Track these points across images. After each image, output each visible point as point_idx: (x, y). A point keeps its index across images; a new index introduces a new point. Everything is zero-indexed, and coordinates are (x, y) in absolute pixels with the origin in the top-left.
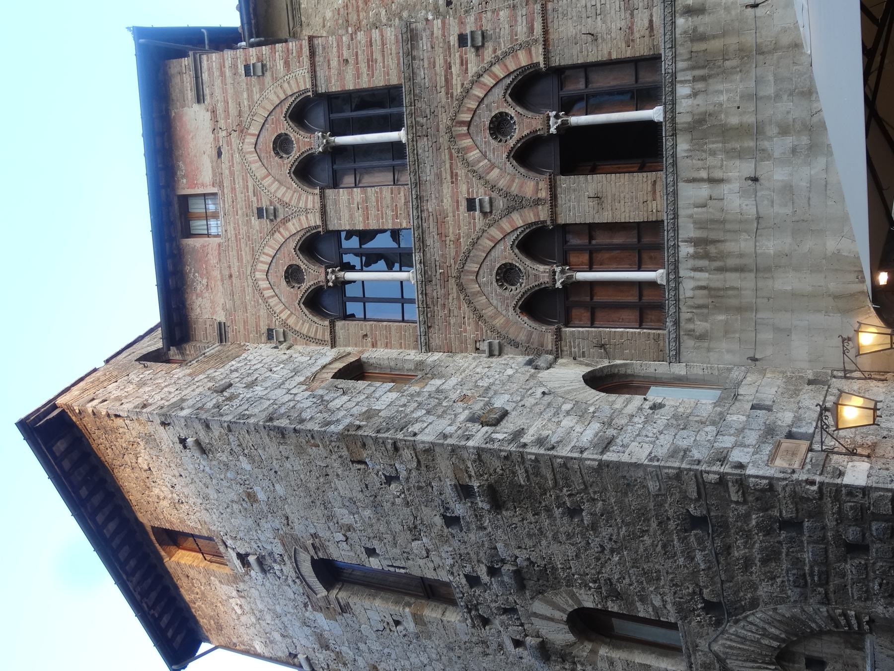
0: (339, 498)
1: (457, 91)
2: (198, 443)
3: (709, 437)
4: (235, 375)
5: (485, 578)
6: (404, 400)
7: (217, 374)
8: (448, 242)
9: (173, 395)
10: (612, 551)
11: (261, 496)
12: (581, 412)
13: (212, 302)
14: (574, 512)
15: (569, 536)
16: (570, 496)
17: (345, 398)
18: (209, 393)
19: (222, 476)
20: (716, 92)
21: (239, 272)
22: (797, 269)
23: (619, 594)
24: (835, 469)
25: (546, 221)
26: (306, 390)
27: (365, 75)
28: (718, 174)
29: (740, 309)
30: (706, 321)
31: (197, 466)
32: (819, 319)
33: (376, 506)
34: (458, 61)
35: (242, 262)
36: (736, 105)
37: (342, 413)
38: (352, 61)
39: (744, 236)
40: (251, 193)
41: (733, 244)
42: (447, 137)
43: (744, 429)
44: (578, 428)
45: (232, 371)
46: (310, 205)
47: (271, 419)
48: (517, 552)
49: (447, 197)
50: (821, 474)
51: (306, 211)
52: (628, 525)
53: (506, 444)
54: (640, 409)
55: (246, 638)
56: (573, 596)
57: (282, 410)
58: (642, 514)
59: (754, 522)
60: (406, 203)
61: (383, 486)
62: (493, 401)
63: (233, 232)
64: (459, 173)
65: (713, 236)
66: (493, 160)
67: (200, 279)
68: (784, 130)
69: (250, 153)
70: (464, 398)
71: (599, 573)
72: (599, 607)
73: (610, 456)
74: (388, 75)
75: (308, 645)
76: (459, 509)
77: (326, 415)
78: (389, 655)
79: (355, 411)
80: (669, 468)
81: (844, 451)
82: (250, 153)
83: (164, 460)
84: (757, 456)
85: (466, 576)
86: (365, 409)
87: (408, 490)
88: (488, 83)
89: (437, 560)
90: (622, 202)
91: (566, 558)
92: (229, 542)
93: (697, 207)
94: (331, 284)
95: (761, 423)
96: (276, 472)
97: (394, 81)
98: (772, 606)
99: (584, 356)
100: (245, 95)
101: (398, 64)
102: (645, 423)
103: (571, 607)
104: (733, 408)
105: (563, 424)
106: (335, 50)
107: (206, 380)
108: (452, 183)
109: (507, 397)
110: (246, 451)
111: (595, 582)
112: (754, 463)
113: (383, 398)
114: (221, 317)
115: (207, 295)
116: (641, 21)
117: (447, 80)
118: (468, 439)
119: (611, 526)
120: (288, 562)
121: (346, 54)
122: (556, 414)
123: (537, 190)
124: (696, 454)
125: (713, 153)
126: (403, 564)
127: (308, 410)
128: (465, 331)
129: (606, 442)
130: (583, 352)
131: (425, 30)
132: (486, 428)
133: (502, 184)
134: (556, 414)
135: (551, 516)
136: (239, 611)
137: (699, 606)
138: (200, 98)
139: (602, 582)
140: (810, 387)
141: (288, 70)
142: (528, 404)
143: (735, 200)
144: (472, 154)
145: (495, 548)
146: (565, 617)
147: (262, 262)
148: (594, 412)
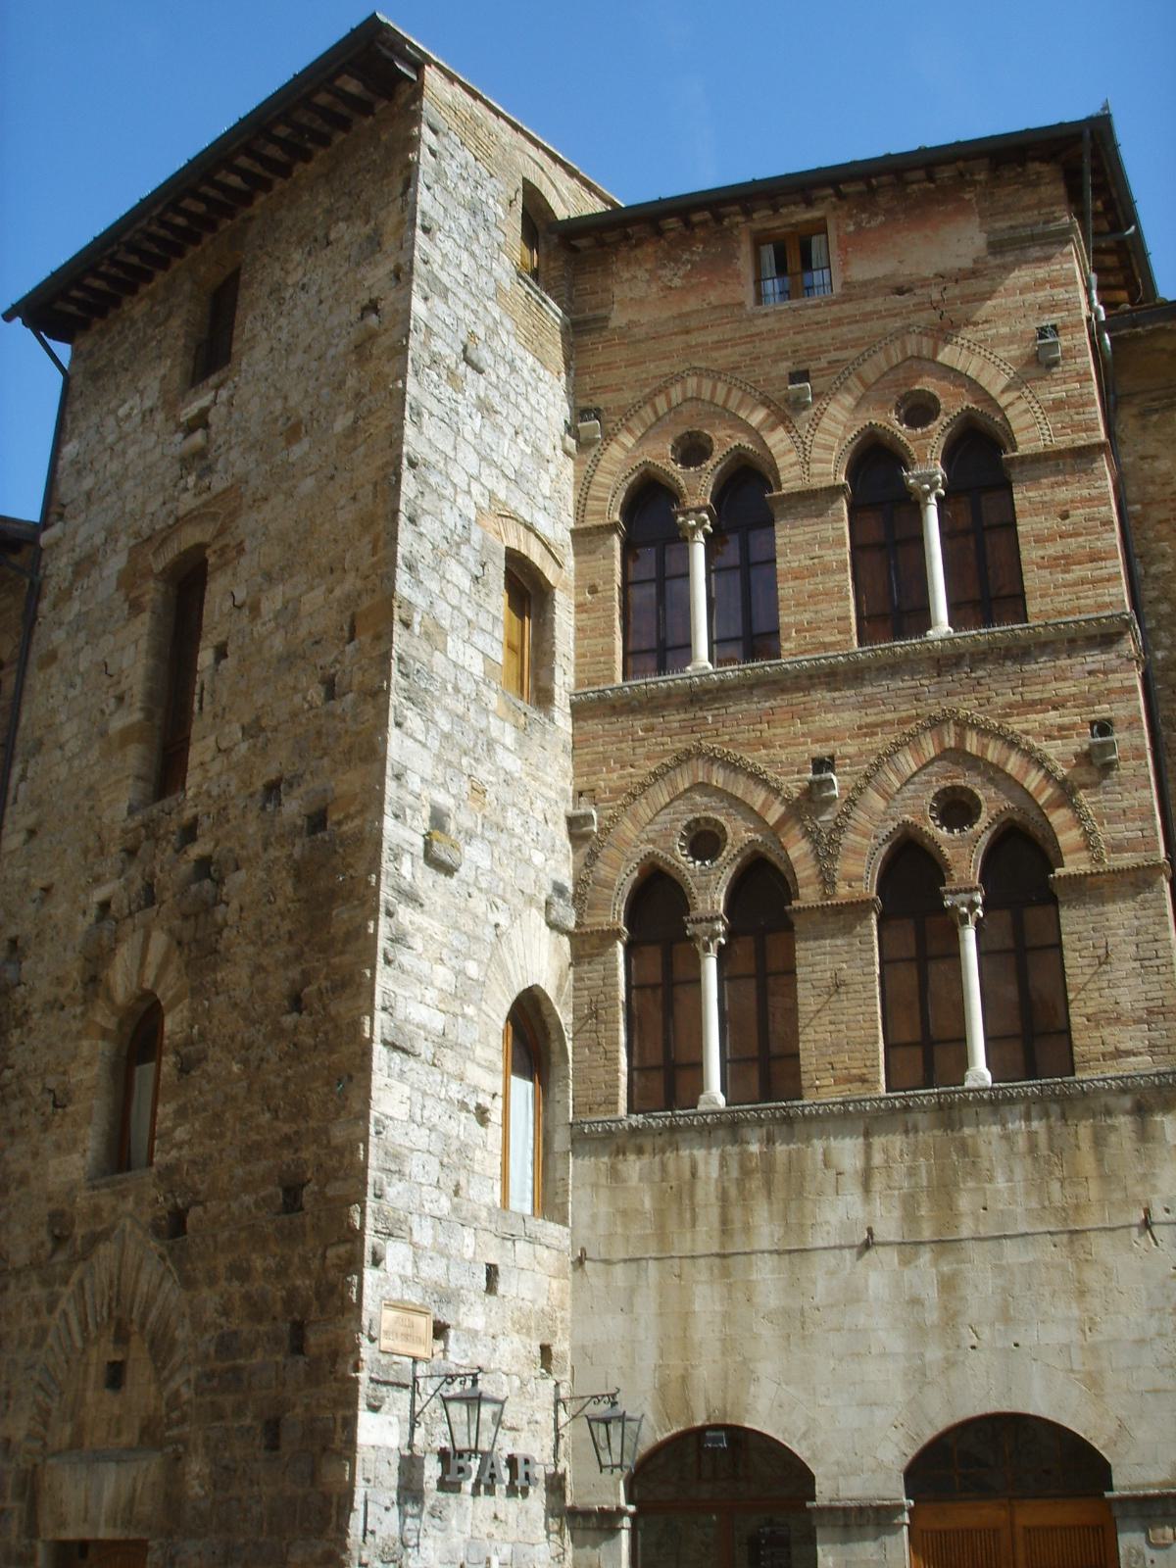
0: (297, 593)
1: (1016, 725)
2: (372, 336)
3: (428, 1206)
4: (503, 371)
5: (196, 851)
6: (468, 688)
7: (504, 337)
8: (759, 726)
9: (453, 272)
10: (245, 1062)
11: (298, 451)
12: (464, 991)
13: (641, 301)
14: (297, 1003)
15: (263, 992)
16: (320, 991)
17: (466, 583)
18: (463, 336)
19: (322, 379)
20: (1011, 1171)
21: (697, 345)
22: (727, 1317)
23: (188, 1072)
24: (382, 1400)
25: (797, 898)
26: (479, 509)
27: (1041, 553)
28: (878, 1182)
29: (662, 1235)
30: (641, 1179)
31: (338, 331)
32: (649, 1357)
33: (289, 659)
34: (1066, 720)
35: (712, 349)
36: (989, 1204)
37: (434, 586)
38: (1066, 526)
39: (779, 1232)
40: (834, 355)
41: (766, 1215)
42: (936, 711)
43: (448, 1257)
44: (431, 995)
45: (511, 364)
46: (816, 468)
47: (413, 465)
48: (235, 904)
49: (836, 721)
50: (372, 1380)
51: (806, 462)
52: (285, 1087)
53: (391, 882)
54: (475, 1090)
55: (83, 425)
56: (177, 999)
57: (433, 479)
58: (300, 1111)
59: (298, 1282)
60: (825, 646)
61: (320, 672)
62: (476, 842)
63: (764, 329)
64: (878, 738)
65: (779, 1178)
66: (891, 800)
67: (681, 273)
68: (948, 1285)
69: (904, 349)
70: (479, 791)
71: (214, 1042)
72: (166, 1042)
73: (379, 1052)
74: (1041, 596)
75: (79, 540)
76: (293, 808)
77: (430, 558)
78: (72, 686)
79: (442, 609)
80: (366, 1151)
81: (417, 1409)
82: (904, 349)
83: (343, 270)
84: (398, 1282)
85: (195, 818)
86: (445, 623)
87: (316, 716)
88: (1029, 779)
89: (215, 767)
90: (832, 1028)
91: (232, 986)
92: (224, 394)
93: (825, 1154)
94: (681, 519)
95: (459, 1283)
96: (332, 478)
97: (1032, 608)
98: (188, 1311)
99: (576, 980)
100: (1004, 330)
101: (1060, 613)
102: (449, 1101)
103: (164, 994)
104: (488, 1237)
105: (439, 968)
106: (1085, 492)
107: (489, 321)
108: (860, 728)
109: (485, 863)
110: (360, 422)
111: (201, 1034)
112: (387, 1279)
113: (470, 651)
114: (618, 319)
115: (654, 288)
116: (1129, 1037)
117: (1033, 704)
118: (397, 817)
119: (281, 1059)
120: (199, 501)
121: (1078, 514)
122: (457, 953)
123: (850, 880)
124: (394, 1191)
125: (912, 1172)
126: (207, 708)
127: (437, 524)
128: (611, 771)
129: (407, 1045)
130: (582, 979)
131: (1119, 657)
132: (420, 842)
133: (860, 816)
134: (457, 953)
135: (286, 963)
136: (121, 412)
137: (179, 1201)
138: (996, 247)
139: (200, 1046)
140: (537, 1352)
141: (1049, 409)
142: (472, 902)
143: (840, 1212)
144: (910, 758)
145: (238, 868)
146: (147, 985)
147: (715, 388)
148: (464, 1016)
